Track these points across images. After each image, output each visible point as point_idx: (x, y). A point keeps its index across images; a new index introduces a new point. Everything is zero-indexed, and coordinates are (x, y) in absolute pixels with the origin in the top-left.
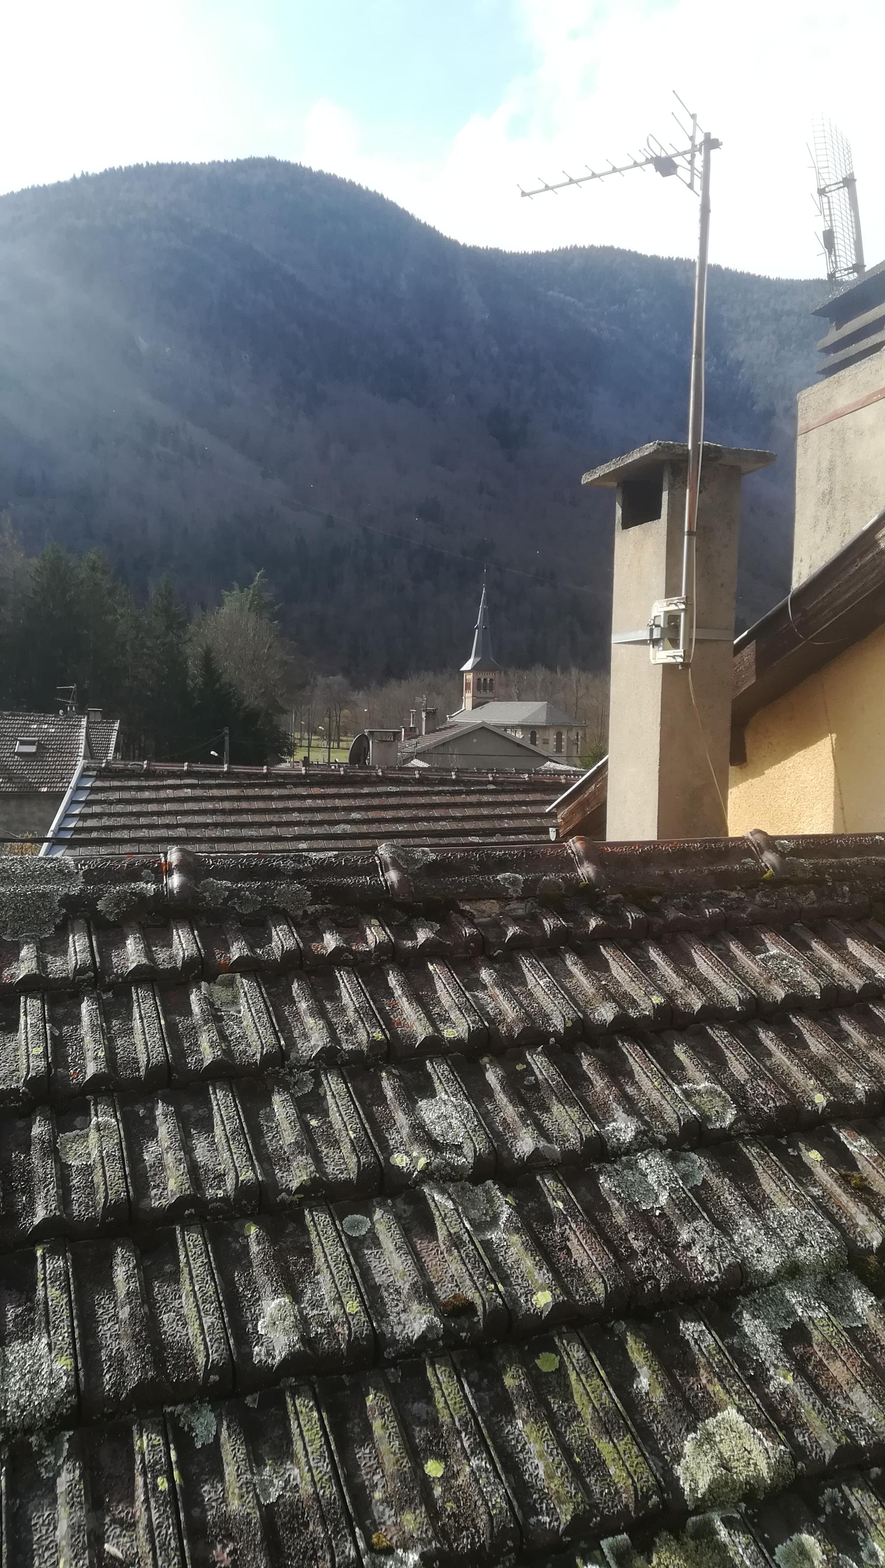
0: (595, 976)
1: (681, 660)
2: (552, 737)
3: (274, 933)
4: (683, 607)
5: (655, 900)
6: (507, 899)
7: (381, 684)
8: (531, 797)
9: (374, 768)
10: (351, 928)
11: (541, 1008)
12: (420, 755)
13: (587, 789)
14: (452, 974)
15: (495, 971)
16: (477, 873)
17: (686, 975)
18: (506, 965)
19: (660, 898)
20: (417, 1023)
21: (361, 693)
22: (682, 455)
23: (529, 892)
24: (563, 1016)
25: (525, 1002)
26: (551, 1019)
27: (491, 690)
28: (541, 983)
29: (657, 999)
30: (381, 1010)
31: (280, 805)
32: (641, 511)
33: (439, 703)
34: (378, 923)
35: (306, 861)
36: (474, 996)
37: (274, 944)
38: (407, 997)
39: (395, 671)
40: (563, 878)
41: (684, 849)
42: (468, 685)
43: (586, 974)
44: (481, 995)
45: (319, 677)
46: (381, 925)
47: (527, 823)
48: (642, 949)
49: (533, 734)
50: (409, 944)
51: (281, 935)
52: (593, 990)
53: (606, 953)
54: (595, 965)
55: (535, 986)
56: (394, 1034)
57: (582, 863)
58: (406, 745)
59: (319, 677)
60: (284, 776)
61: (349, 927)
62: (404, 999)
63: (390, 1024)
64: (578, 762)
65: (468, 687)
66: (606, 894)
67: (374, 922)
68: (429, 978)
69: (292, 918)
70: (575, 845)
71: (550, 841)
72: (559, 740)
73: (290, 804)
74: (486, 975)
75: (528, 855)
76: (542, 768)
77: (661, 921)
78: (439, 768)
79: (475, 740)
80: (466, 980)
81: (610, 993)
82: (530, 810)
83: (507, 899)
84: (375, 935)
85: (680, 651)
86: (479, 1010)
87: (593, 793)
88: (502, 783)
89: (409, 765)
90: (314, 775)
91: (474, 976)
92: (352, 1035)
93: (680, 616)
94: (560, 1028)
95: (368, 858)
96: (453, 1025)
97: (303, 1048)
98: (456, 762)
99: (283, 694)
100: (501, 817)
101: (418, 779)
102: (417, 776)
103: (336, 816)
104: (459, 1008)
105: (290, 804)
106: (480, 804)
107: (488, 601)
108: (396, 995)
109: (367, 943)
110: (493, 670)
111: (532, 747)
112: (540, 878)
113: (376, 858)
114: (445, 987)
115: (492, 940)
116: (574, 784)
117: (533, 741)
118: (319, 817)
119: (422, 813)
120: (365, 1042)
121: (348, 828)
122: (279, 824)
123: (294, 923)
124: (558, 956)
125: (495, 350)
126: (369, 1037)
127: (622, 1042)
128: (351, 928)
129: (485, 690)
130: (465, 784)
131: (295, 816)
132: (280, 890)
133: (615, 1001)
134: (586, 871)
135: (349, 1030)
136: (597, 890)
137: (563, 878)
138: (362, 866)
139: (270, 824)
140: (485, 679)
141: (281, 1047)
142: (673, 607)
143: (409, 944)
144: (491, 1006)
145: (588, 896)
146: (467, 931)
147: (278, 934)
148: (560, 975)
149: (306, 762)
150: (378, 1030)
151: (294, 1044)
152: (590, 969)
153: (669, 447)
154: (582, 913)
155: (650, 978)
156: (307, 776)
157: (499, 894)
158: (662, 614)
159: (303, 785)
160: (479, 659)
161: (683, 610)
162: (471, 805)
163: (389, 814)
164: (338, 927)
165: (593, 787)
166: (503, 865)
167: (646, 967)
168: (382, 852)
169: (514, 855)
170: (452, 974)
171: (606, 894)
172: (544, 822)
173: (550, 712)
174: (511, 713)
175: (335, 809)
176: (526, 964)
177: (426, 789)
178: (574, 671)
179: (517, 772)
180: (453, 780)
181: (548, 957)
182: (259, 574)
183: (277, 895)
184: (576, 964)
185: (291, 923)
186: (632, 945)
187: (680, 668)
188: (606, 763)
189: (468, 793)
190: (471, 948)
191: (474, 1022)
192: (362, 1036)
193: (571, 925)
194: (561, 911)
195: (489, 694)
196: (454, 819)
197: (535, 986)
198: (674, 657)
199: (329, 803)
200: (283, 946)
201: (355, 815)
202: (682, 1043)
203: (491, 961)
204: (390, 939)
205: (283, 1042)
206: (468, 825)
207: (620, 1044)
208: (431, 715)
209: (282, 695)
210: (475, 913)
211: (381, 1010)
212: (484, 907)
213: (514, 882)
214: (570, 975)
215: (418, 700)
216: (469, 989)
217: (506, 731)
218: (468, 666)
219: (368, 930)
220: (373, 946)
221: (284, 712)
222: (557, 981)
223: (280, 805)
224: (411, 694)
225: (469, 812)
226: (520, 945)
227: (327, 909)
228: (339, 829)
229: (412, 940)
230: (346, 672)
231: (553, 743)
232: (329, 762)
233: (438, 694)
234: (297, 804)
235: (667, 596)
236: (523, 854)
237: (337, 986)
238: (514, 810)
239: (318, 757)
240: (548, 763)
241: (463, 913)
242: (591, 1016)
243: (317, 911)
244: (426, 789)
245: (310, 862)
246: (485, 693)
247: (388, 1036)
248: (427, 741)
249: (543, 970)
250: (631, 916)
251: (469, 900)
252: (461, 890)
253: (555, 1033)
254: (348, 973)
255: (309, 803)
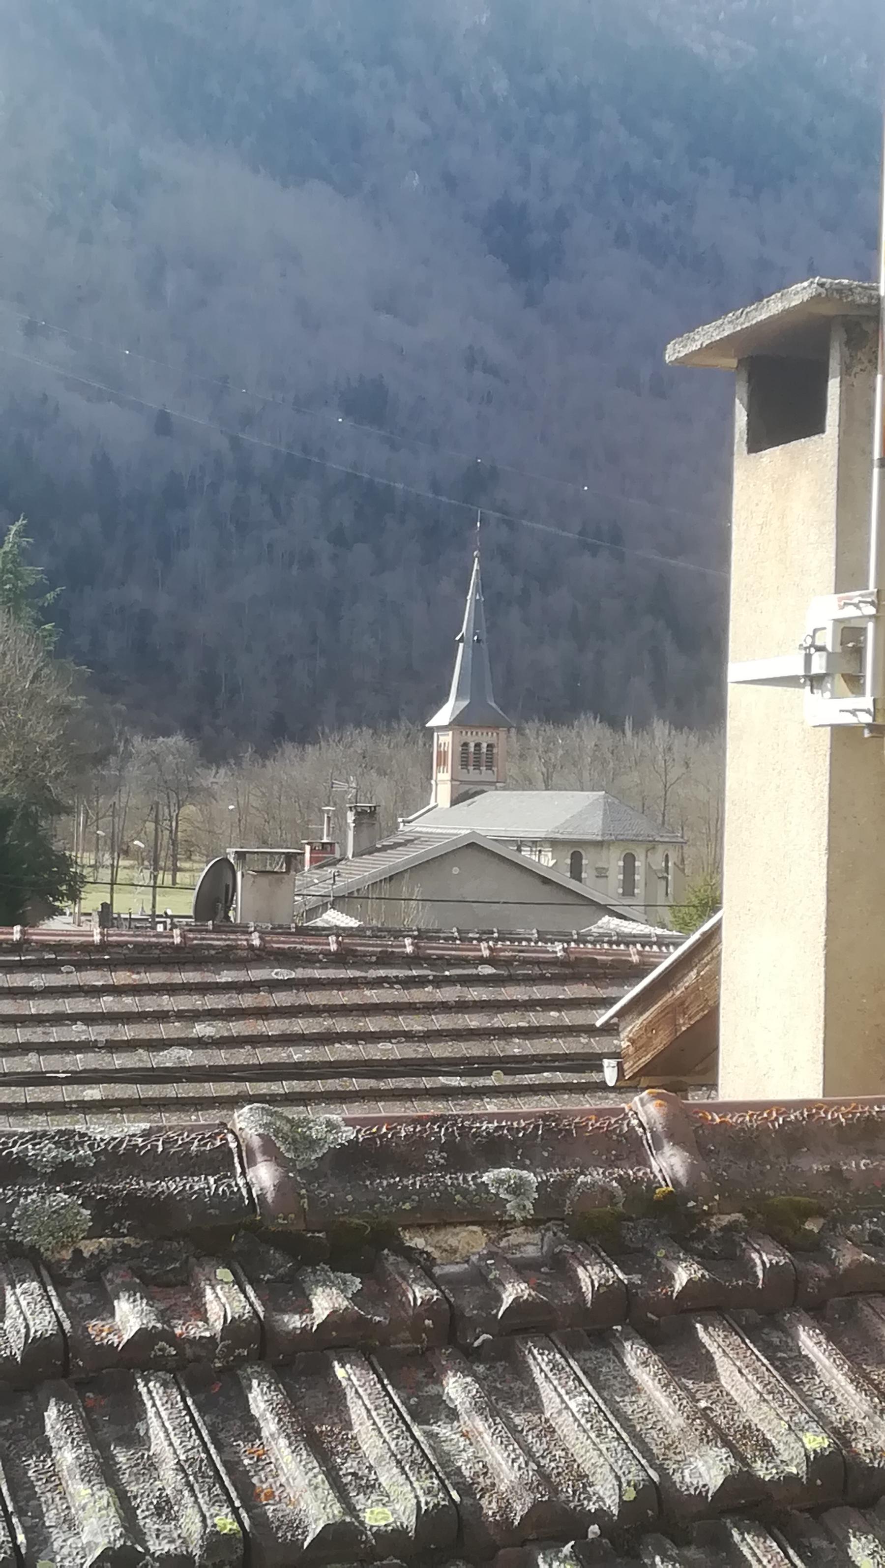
0: (685, 1388)
1: (868, 719)
2: (615, 863)
3: (10, 1300)
4: (872, 611)
5: (812, 1226)
6: (503, 1223)
7: (264, 753)
8: (569, 992)
9: (244, 930)
10: (171, 1287)
11: (571, 1461)
12: (340, 901)
13: (681, 979)
14: (384, 1387)
15: (477, 1380)
16: (441, 1168)
17: (876, 1387)
18: (500, 1365)
19: (822, 1221)
20: (308, 1496)
21: (222, 771)
22: (868, 306)
23: (549, 1209)
24: (618, 1478)
25: (538, 1448)
26: (591, 1485)
27: (489, 767)
28: (572, 1404)
29: (816, 1441)
30: (232, 1466)
31: (47, 1007)
32: (786, 414)
33: (382, 793)
34: (231, 1278)
35: (82, 1144)
36: (430, 1435)
37: (8, 1322)
38: (288, 1436)
39: (289, 727)
40: (620, 1180)
41: (870, 1118)
42: (442, 756)
43: (667, 1385)
44: (443, 1430)
45: (137, 740)
46: (237, 1281)
47: (561, 1046)
48: (784, 1331)
49: (576, 858)
50: (295, 1322)
51: (24, 1303)
52: (681, 1421)
53: (711, 1339)
54: (686, 1364)
55: (560, 1413)
56: (260, 1520)
57: (659, 1147)
58: (313, 881)
59: (137, 740)
60: (58, 948)
61: (169, 1285)
62: (283, 1442)
63: (250, 1496)
64: (667, 915)
65: (442, 761)
66: (709, 1214)
67: (224, 1273)
68: (336, 1396)
69: (49, 1266)
70: (646, 1109)
71: (602, 1086)
72: (629, 869)
73: (68, 1006)
74: (456, 1388)
75: (548, 1130)
76: (593, 929)
77: (824, 1272)
78: (380, 930)
79: (456, 870)
80: (413, 1401)
81: (717, 1427)
82: (568, 1018)
83: (504, 1225)
84: (224, 1302)
85: (867, 701)
86: (443, 1467)
87: (693, 990)
88: (508, 963)
89: (319, 922)
90: (119, 945)
91: (432, 1389)
92: (169, 1520)
93: (864, 630)
94: (611, 1504)
95: (213, 1137)
96: (386, 1499)
97: (65, 1551)
98: (417, 916)
99: (62, 774)
100: (506, 1033)
101: (335, 954)
102: (333, 947)
103: (162, 1031)
104: (399, 1462)
105: (68, 1006)
106: (462, 1007)
107: (484, 586)
108: (265, 1433)
109: (206, 1321)
110: (495, 726)
111: (573, 885)
112: (570, 1181)
113: (230, 1137)
114: (370, 1416)
115: (470, 1312)
116: (656, 965)
117: (576, 872)
118: (127, 1032)
119: (343, 1025)
120: (196, 1536)
121: (188, 1057)
122: (44, 1048)
123: (56, 1278)
124: (608, 1345)
125: (501, 86)
126: (205, 1526)
127: (742, 1534)
128: (171, 1287)
129: (477, 766)
130: (432, 963)
131: (78, 1032)
132: (25, 1208)
133: (727, 1444)
134: (669, 1164)
135: (164, 1509)
136: (691, 1204)
137: (620, 1180)
138: (200, 1154)
139: (25, 1048)
140: (478, 745)
141: (16, 1548)
142: (850, 612)
143: (295, 1322)
144: (465, 1455)
145: (673, 1218)
146: (419, 1293)
147: (17, 1302)
148: (609, 1385)
149: (106, 915)
150: (226, 1510)
151: (47, 1541)
152: (673, 1373)
153: (841, 289)
154: (661, 1254)
155: (801, 1393)
156: (104, 946)
157: (487, 1215)
158: (830, 626)
159: (97, 965)
160: (465, 703)
161: (871, 617)
162: (444, 1007)
163: (274, 1027)
164: (149, 1286)
165: (693, 974)
166: (495, 1149)
167: (791, 1367)
168: (243, 1125)
169: (518, 1130)
170: (384, 1387)
171: (709, 1214)
172: (596, 1045)
173: (610, 811)
174: (530, 815)
175: (161, 1016)
176: (540, 1363)
177: (351, 973)
178: (660, 729)
179: (542, 937)
180: (407, 956)
181: (588, 1348)
182: (14, 528)
183: (19, 1218)
184: (645, 1364)
185: (47, 1279)
186: (762, 1318)
187: (867, 734)
188: (717, 927)
189: (439, 982)
190: (426, 1329)
191: (429, 1491)
192: (190, 1524)
193: (636, 1279)
194: (617, 1251)
195: (485, 775)
196: (409, 1036)
197: (560, 1413)
198: (854, 712)
199: (150, 1003)
200: (27, 1327)
201: (202, 1029)
202: (865, 1533)
203: (468, 1358)
204: (255, 1312)
205: (21, 1538)
206: (439, 1050)
207: (737, 1537)
208: (366, 817)
209: (58, 775)
210: (436, 1254)
211: (232, 1466)
212: (453, 1242)
213: (518, 1189)
214: (632, 1387)
215: (340, 786)
216: (420, 1417)
217: (519, 850)
218: (443, 716)
219: (208, 1291)
220: (219, 1326)
221: (58, 809)
222: (605, 1401)
223: (47, 1007)
224: (327, 772)
225: (440, 1022)
226: (529, 1323)
227: (124, 1246)
228: (168, 1058)
229: (301, 1313)
230: (192, 729)
231: (616, 876)
232: (154, 915)
233: (382, 772)
234: (81, 1005)
235: (837, 591)
236: (536, 1127)
237: (141, 1415)
238: (534, 1019)
239: (130, 904)
240: (606, 918)
241: (410, 1255)
242: (677, 1477)
243: (101, 1251)
244: (351, 973)
245: (91, 1147)
246: (478, 770)
247: (247, 1523)
248: (358, 871)
249: (577, 1378)
250: (763, 1259)
251: (423, 1227)
252: (407, 1206)
253: (600, 1515)
254: (165, 1385)
255: (107, 1003)
